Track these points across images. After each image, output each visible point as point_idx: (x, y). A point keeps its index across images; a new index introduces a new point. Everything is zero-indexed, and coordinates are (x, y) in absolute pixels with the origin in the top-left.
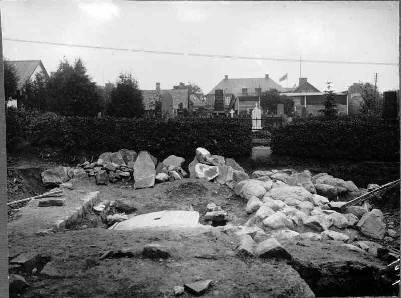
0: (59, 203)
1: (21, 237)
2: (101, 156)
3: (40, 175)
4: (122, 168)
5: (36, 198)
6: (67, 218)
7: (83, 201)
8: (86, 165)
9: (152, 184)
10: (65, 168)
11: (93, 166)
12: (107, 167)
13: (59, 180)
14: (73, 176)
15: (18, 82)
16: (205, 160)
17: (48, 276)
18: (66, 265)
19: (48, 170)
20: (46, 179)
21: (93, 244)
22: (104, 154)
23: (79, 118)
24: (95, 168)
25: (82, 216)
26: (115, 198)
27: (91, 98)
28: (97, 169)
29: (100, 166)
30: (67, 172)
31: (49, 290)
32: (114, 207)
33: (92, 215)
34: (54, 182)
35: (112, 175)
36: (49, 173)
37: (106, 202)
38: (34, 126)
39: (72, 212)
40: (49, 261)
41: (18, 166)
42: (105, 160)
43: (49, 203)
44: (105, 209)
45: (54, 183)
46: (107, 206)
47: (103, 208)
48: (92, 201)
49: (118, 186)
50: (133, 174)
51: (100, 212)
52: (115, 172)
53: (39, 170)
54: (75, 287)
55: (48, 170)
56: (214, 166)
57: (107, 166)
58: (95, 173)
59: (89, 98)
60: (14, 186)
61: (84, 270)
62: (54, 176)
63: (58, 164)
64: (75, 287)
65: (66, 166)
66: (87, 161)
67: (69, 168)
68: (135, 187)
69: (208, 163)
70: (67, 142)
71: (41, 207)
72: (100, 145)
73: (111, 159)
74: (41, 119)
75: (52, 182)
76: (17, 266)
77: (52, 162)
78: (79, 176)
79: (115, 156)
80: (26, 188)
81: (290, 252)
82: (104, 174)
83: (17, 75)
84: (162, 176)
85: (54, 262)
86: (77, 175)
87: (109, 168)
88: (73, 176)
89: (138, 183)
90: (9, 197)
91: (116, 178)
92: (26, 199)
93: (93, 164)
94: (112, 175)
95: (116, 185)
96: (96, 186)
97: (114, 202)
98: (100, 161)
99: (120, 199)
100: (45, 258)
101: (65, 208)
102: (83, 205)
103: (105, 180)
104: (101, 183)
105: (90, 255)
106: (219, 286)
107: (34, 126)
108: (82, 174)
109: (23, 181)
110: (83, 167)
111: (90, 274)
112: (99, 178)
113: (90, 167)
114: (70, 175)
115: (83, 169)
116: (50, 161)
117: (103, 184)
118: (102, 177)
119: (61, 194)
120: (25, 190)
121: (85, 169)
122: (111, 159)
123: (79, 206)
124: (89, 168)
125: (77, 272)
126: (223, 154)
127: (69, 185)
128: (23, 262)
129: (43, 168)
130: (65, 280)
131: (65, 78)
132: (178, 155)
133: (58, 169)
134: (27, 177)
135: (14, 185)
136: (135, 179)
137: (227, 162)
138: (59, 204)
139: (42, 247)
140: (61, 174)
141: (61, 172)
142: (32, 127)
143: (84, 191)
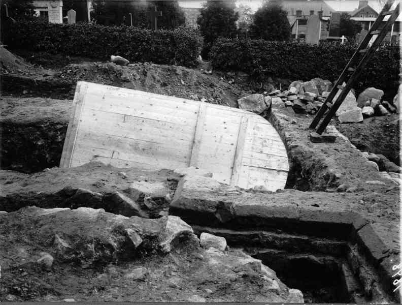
9: (361, 119)
84: (369, 110)
89: (343, 117)
93: (287, 92)
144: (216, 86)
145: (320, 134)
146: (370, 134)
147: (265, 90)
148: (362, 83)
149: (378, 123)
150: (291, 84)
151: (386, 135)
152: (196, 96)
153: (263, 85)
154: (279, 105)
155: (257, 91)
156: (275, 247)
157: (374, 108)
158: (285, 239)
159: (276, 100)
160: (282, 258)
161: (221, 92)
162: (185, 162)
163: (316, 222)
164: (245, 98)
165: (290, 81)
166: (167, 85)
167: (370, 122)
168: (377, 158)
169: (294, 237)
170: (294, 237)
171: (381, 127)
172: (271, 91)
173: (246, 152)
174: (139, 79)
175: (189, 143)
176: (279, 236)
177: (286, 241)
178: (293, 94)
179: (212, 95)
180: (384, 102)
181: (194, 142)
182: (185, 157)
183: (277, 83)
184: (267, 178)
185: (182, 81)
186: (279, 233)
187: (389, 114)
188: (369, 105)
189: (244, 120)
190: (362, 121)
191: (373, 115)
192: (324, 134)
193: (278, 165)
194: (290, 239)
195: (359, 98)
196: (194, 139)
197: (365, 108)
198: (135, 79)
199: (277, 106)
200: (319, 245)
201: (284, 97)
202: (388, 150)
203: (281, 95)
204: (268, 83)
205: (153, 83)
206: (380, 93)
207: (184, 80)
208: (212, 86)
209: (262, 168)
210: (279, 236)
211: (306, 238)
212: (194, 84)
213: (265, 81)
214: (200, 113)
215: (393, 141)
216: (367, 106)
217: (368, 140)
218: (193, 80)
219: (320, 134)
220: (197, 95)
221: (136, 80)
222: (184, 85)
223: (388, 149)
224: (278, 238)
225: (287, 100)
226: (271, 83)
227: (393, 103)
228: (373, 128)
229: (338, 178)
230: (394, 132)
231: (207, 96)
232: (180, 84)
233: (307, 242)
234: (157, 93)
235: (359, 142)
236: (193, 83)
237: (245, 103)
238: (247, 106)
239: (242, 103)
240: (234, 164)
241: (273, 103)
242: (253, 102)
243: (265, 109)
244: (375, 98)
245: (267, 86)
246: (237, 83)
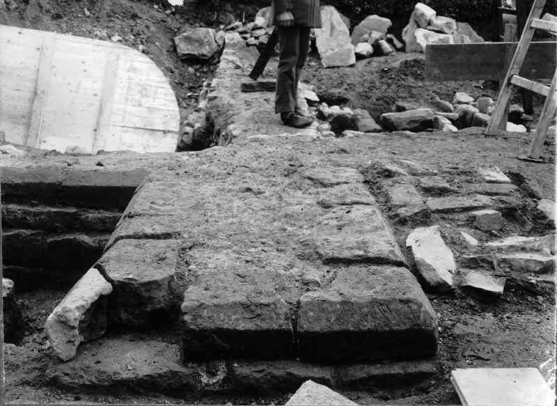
9: (353, 60)
16: (429, 23)
30: (215, 38)
43: (257, 86)
45: (195, 55)
50: (315, 43)
56: (446, 34)
68: (324, 64)
69: (436, 29)
81: (383, 229)
84: (365, 48)
89: (328, 58)
93: (250, 25)
106: (352, 215)
108: (239, 42)
126: (454, 15)
132: (382, 15)
136: (319, 51)
137: (460, 29)
140: (206, 40)
144: (141, 18)
145: (255, 80)
146: (359, 83)
147: (222, 23)
148: (360, 9)
149: (375, 66)
150: (259, 13)
151: (382, 83)
152: (104, 33)
153: (218, 15)
154: (236, 45)
155: (210, 24)
156: (27, 226)
157: (372, 45)
158: (42, 213)
159: (234, 37)
160: (38, 241)
161: (147, 27)
162: (24, 124)
163: (86, 187)
164: (185, 34)
165: (258, 9)
166: (61, 17)
167: (365, 66)
168: (349, 114)
169: (55, 210)
170: (55, 210)
171: (377, 72)
172: (229, 23)
173: (118, 104)
174: (16, 8)
175: (29, 95)
176: (32, 210)
177: (43, 217)
178: (260, 28)
179: (132, 31)
180: (389, 36)
181: (36, 93)
182: (23, 117)
183: (239, 12)
184: (148, 143)
185: (85, 9)
186: (33, 205)
187: (394, 53)
188: (367, 41)
189: (113, 58)
190: (354, 64)
191: (371, 55)
192: (260, 80)
193: (164, 123)
194: (49, 213)
195: (354, 31)
196: (36, 89)
197: (360, 44)
198: (8, 8)
199: (234, 45)
200: (92, 219)
201: (245, 32)
202: (381, 105)
203: (241, 29)
204: (225, 11)
205: (37, 13)
206: (385, 23)
207: (88, 10)
208: (134, 17)
209: (140, 128)
210: (32, 210)
211: (73, 210)
212: (105, 15)
213: (221, 9)
214: (45, 50)
215: (390, 91)
216: (363, 42)
217: (353, 90)
218: (105, 9)
219: (255, 80)
220: (105, 31)
221: (9, 9)
222: (89, 17)
223: (381, 102)
224: (32, 212)
225: (251, 37)
226: (230, 12)
227: (401, 37)
228: (365, 73)
229: (235, 137)
230: (394, 78)
231: (122, 32)
232: (82, 16)
233: (75, 217)
234: (43, 30)
235: (340, 93)
236: (104, 12)
237: (185, 42)
238: (189, 47)
239: (180, 42)
240: (98, 123)
241: (226, 41)
242: (197, 41)
243: (215, 50)
244: (376, 30)
245: (224, 17)
246: (179, 13)
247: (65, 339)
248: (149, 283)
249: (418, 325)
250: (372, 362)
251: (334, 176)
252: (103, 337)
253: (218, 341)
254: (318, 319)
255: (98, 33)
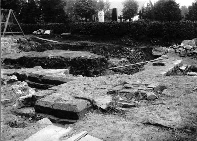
0: (162, 64)
1: (149, 77)
2: (183, 42)
3: (152, 51)
4: (194, 48)
5: (151, 61)
6: (167, 71)
7: (174, 64)
8: (174, 46)
10: (164, 48)
11: (179, 47)
12: (186, 48)
13: (160, 54)
14: (168, 52)
15: (138, 8)
17: (166, 95)
18: (174, 91)
19: (155, 49)
20: (154, 53)
21: (187, 83)
22: (185, 41)
23: (172, 22)
24: (179, 48)
25: (174, 71)
26: (191, 64)
27: (177, 12)
28: (180, 49)
29: (182, 47)
30: (165, 50)
31: (168, 102)
32: (190, 69)
33: (179, 71)
34: (158, 55)
35: (189, 52)
36: (156, 50)
37: (186, 65)
38: (148, 27)
39: (169, 68)
40: (166, 88)
41: (141, 46)
42: (185, 44)
44: (186, 69)
45: (158, 55)
46: (187, 67)
47: (184, 68)
48: (179, 64)
49: (192, 58)
51: (183, 70)
52: (190, 50)
53: (152, 49)
54: (181, 102)
55: (155, 49)
57: (186, 47)
58: (179, 51)
59: (176, 12)
60: (139, 56)
61: (185, 95)
62: (158, 52)
63: (160, 46)
64: (181, 102)
65: (164, 47)
66: (175, 44)
67: (165, 48)
70: (165, 35)
71: (153, 65)
72: (182, 36)
73: (188, 43)
74: (152, 23)
75: (157, 54)
76: (151, 88)
77: (157, 45)
78: (171, 52)
79: (191, 42)
80: (145, 57)
82: (184, 51)
83: (138, 5)
85: (168, 89)
86: (170, 51)
87: (187, 48)
88: (168, 52)
90: (138, 61)
91: (191, 53)
92: (139, 63)
94: (189, 52)
95: (190, 57)
96: (180, 57)
97: (190, 66)
98: (182, 45)
99: (194, 65)
100: (163, 87)
101: (166, 67)
102: (175, 66)
103: (185, 55)
104: (183, 56)
105: (187, 88)
107: (148, 27)
108: (173, 51)
109: (144, 54)
110: (173, 47)
111: (188, 97)
112: (182, 53)
113: (176, 47)
114: (166, 52)
115: (173, 49)
116: (156, 44)
117: (183, 57)
118: (183, 53)
119: (162, 60)
120: (145, 58)
121: (174, 49)
122: (188, 43)
123: (173, 66)
124: (176, 48)
125: (181, 95)
127: (166, 56)
128: (154, 87)
129: (153, 48)
130: (175, 98)
131: (162, 3)
133: (160, 48)
134: (145, 52)
135: (140, 55)
138: (163, 65)
139: (160, 81)
141: (162, 50)
142: (148, 28)
143: (174, 59)
247: (18, 104)
248: (38, 96)
249: (74, 111)
250: (66, 118)
251: (125, 83)
252: (29, 107)
253: (40, 109)
254: (57, 106)
255: (128, 49)
